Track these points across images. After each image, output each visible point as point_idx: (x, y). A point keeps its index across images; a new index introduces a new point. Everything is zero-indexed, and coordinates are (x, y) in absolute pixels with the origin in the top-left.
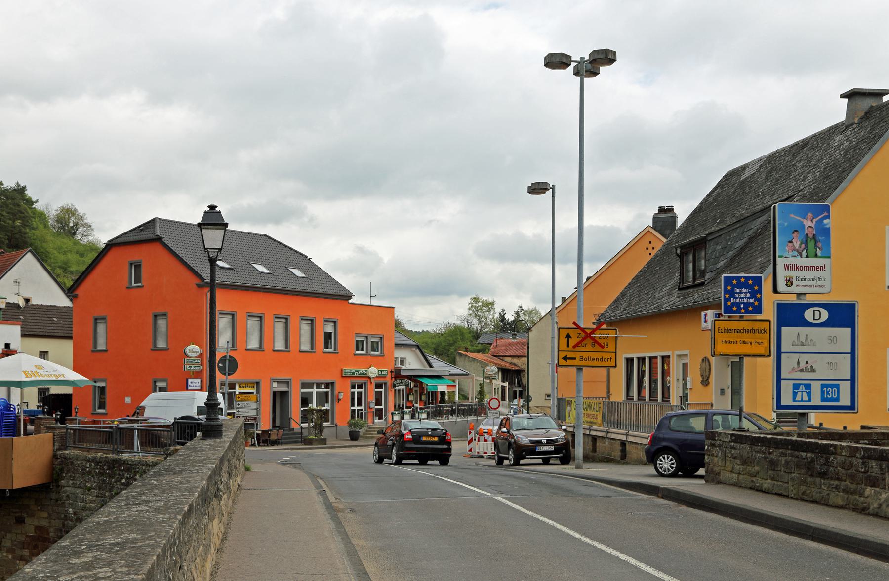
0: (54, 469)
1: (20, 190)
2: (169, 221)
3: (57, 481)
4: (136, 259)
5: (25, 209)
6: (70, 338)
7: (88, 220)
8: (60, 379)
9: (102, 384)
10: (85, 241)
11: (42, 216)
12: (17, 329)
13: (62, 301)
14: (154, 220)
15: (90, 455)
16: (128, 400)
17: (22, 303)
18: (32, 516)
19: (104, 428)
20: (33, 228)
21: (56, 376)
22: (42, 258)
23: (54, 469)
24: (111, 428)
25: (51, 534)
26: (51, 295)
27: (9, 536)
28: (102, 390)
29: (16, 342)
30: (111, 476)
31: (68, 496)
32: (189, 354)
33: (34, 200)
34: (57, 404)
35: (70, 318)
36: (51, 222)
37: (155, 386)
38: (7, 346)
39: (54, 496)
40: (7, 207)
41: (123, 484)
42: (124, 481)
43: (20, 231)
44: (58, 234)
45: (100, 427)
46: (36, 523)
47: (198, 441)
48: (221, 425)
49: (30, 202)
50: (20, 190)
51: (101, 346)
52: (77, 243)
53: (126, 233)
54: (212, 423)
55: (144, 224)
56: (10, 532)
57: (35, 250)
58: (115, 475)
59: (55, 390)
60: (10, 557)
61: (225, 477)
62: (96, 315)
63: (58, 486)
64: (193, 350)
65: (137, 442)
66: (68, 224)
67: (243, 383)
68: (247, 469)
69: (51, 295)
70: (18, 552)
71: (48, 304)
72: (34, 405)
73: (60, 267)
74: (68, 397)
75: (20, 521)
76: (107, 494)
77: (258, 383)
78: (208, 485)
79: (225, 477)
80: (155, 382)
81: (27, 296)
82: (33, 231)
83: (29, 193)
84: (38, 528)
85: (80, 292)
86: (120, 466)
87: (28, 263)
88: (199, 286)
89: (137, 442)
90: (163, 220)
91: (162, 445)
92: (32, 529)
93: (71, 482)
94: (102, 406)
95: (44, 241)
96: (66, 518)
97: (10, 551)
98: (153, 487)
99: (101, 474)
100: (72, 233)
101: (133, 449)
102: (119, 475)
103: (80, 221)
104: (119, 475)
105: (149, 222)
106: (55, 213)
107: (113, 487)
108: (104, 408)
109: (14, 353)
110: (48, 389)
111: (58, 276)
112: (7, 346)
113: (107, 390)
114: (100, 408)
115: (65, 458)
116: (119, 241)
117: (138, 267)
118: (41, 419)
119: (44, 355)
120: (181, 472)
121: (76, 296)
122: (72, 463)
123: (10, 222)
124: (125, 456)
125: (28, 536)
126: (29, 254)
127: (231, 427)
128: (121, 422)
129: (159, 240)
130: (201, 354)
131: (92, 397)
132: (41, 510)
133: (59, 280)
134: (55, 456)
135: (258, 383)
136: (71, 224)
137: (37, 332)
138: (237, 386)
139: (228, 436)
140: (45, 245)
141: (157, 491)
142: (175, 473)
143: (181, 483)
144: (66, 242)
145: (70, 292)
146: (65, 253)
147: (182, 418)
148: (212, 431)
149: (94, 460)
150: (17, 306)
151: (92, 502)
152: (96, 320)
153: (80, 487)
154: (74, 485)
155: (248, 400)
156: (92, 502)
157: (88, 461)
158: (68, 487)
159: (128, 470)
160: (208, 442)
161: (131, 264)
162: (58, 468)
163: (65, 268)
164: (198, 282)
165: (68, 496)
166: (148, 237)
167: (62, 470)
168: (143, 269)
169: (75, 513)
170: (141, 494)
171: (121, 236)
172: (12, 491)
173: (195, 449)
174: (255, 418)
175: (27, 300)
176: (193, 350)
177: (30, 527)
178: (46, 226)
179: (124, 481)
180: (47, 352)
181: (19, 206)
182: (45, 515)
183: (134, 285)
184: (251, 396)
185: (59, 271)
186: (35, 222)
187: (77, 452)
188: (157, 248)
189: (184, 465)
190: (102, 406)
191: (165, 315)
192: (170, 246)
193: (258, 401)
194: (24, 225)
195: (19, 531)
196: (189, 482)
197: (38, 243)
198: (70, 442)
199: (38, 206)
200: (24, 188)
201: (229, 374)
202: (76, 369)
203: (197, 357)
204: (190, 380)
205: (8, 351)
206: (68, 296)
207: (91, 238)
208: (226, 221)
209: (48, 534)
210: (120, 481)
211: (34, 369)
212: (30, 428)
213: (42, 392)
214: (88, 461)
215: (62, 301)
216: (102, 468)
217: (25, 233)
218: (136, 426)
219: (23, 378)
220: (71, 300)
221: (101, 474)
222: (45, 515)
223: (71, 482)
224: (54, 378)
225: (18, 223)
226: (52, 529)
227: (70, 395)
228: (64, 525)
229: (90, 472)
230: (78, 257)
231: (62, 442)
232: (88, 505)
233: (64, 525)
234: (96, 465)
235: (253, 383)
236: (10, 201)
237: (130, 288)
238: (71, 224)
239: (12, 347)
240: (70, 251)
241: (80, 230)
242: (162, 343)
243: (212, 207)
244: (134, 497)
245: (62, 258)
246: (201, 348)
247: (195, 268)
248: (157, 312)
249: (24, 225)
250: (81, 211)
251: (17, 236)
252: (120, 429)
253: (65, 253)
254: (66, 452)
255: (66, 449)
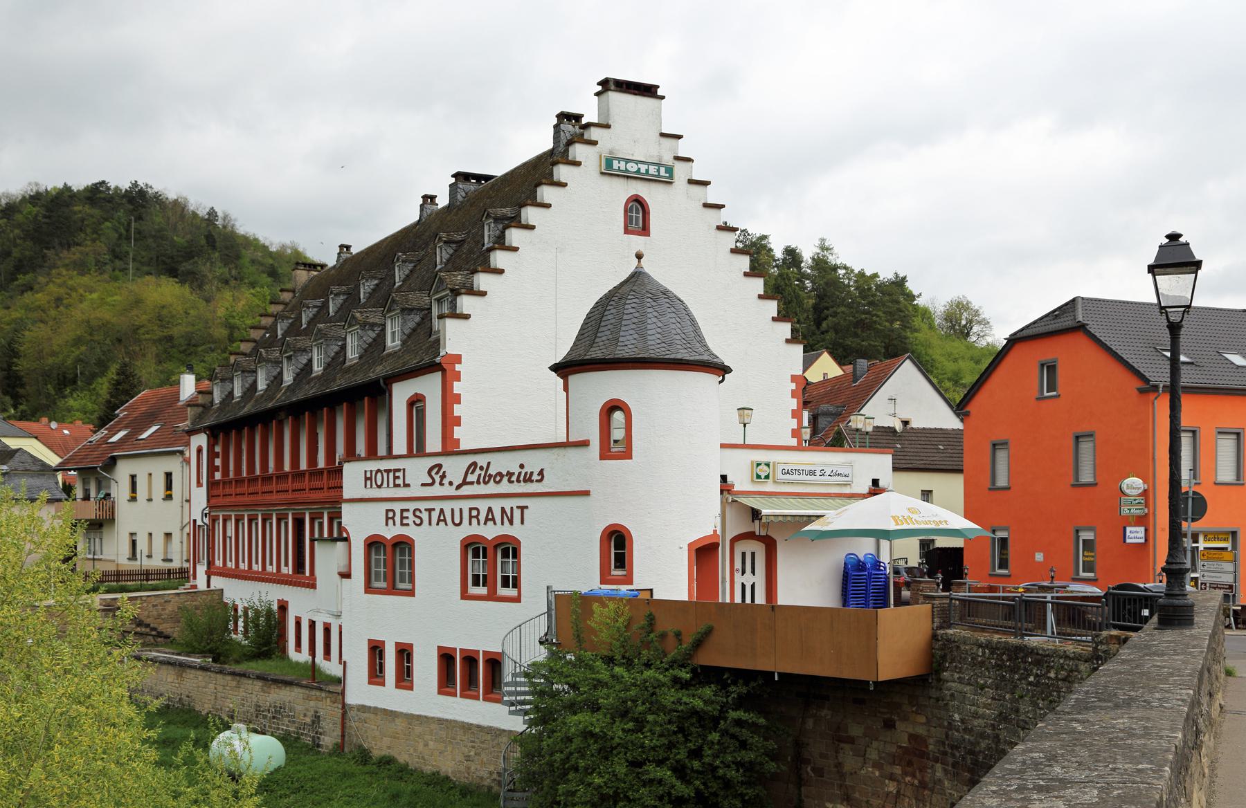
0: (933, 656)
1: (900, 283)
2: (1096, 300)
3: (938, 672)
4: (1048, 357)
5: (906, 307)
6: (960, 471)
7: (985, 314)
8: (941, 527)
9: (1004, 534)
10: (983, 343)
11: (925, 314)
12: (886, 460)
13: (948, 420)
14: (1074, 300)
15: (983, 637)
16: (1039, 557)
17: (898, 426)
18: (905, 719)
19: (1004, 598)
20: (916, 331)
21: (937, 523)
22: (925, 368)
23: (933, 656)
24: (1013, 599)
25: (931, 747)
26: (934, 414)
27: (875, 744)
28: (1004, 542)
29: (886, 475)
30: (1013, 670)
31: (952, 695)
32: (1128, 491)
33: (915, 293)
34: (943, 562)
35: (960, 443)
36: (937, 321)
37: (1078, 537)
38: (875, 482)
39: (934, 693)
40: (884, 305)
41: (1030, 683)
42: (1031, 679)
43: (899, 336)
44: (947, 336)
45: (998, 598)
46: (910, 730)
47: (1149, 635)
48: (1192, 606)
49: (911, 297)
50: (900, 283)
51: (1002, 481)
52: (971, 346)
53: (1034, 323)
54: (1176, 602)
55: (1059, 308)
56: (876, 739)
57: (918, 358)
58: (1019, 668)
59: (941, 542)
60: (877, 774)
61: (1205, 699)
62: (995, 439)
63: (939, 680)
64: (1133, 484)
65: (1050, 618)
66: (960, 322)
67: (1212, 533)
68: (1229, 673)
69: (934, 414)
70: (888, 769)
71: (933, 427)
72: (914, 560)
73: (949, 379)
74: (959, 551)
75: (889, 725)
76: (1008, 696)
77: (1234, 534)
78: (1185, 736)
79: (1205, 699)
80: (1077, 531)
81: (905, 417)
82: (916, 334)
83: (911, 286)
84: (913, 737)
85: (972, 408)
86: (1027, 656)
87: (906, 376)
88: (1141, 391)
89: (1050, 618)
90: (1088, 299)
91: (1092, 626)
92: (906, 737)
93: (956, 676)
94: (1004, 564)
95: (930, 346)
96: (951, 726)
97: (877, 765)
98: (1077, 739)
99: (1000, 667)
100: (965, 333)
101: (1045, 629)
102: (1025, 669)
103: (975, 317)
104: (1025, 669)
105: (1066, 304)
106: (942, 309)
107: (1016, 687)
108: (1006, 568)
109: (883, 491)
110: (933, 541)
111: (946, 390)
112: (875, 482)
113: (1010, 543)
114: (1000, 567)
115: (949, 640)
116: (1024, 333)
117: (1052, 369)
118: (920, 582)
119: (927, 495)
120: (1129, 703)
121: (967, 414)
122: (958, 647)
123: (887, 324)
124: (1034, 641)
125: (900, 747)
126: (908, 362)
127: (1207, 607)
128: (1027, 590)
129: (1081, 328)
130: (1145, 491)
131: (989, 552)
132: (917, 713)
133: (947, 396)
134: (934, 637)
135: (1234, 534)
136: (964, 322)
137: (918, 464)
138: (1201, 538)
139: (1205, 621)
140: (930, 351)
141: (1084, 753)
142: (1117, 706)
143: (1130, 734)
144: (957, 346)
145: (960, 408)
146: (956, 360)
147: (1120, 587)
148: (1175, 615)
149: (988, 645)
150: (892, 431)
151: (986, 706)
152: (994, 445)
153: (969, 684)
154: (961, 680)
155: (1220, 560)
156: (986, 706)
157: (980, 646)
158: (953, 681)
159: (1038, 663)
160: (1170, 635)
161: (1042, 365)
162: (939, 654)
163: (956, 380)
164: (1140, 385)
165: (952, 695)
166: (1067, 324)
167: (944, 657)
168: (1060, 371)
169: (962, 721)
170: (1052, 758)
171: (1028, 326)
172: (876, 683)
173: (1147, 650)
174: (1231, 587)
175: (906, 423)
176: (1133, 484)
177: (903, 732)
178: (931, 327)
179: (1031, 679)
180: (931, 491)
181: (898, 302)
182: (923, 719)
183: (1046, 394)
184: (1224, 554)
185: (948, 384)
186: (917, 322)
187: (966, 633)
188: (1080, 340)
189: (1132, 684)
190: (1004, 564)
191: (1091, 435)
192: (1098, 335)
193: (1234, 561)
194: (904, 327)
195: (888, 739)
196: (1147, 733)
197: (921, 349)
198: (955, 617)
199: (919, 302)
200: (904, 279)
201: (1193, 520)
202: (968, 515)
203: (1140, 495)
204: (1128, 529)
205: (876, 488)
206: (958, 415)
207: (989, 339)
208: (1198, 257)
209: (927, 747)
210: (1026, 679)
211: (906, 514)
212: (906, 594)
213: (925, 545)
214: (980, 646)
215: (948, 420)
216: (999, 658)
217: (906, 338)
218: (1049, 596)
219: (892, 526)
220: (962, 420)
221: (1000, 667)
222: (923, 719)
223: (956, 676)
224: (933, 526)
225: (897, 325)
226: (931, 741)
227: (961, 550)
228: (947, 736)
229: (983, 663)
230: (972, 364)
231: (944, 617)
232: (981, 711)
233: (947, 736)
234: (992, 653)
235: (1227, 533)
236: (887, 298)
237: (1041, 399)
238: (964, 322)
239: (881, 484)
240: (963, 358)
241: (975, 329)
242: (1087, 476)
243: (1174, 237)
244: (1036, 765)
245: (950, 366)
246: (1145, 482)
247: (1136, 365)
248: (1079, 431)
249: (904, 327)
250: (975, 305)
251: (895, 342)
252: (1026, 602)
253: (956, 360)
254: (950, 632)
255: (949, 627)
